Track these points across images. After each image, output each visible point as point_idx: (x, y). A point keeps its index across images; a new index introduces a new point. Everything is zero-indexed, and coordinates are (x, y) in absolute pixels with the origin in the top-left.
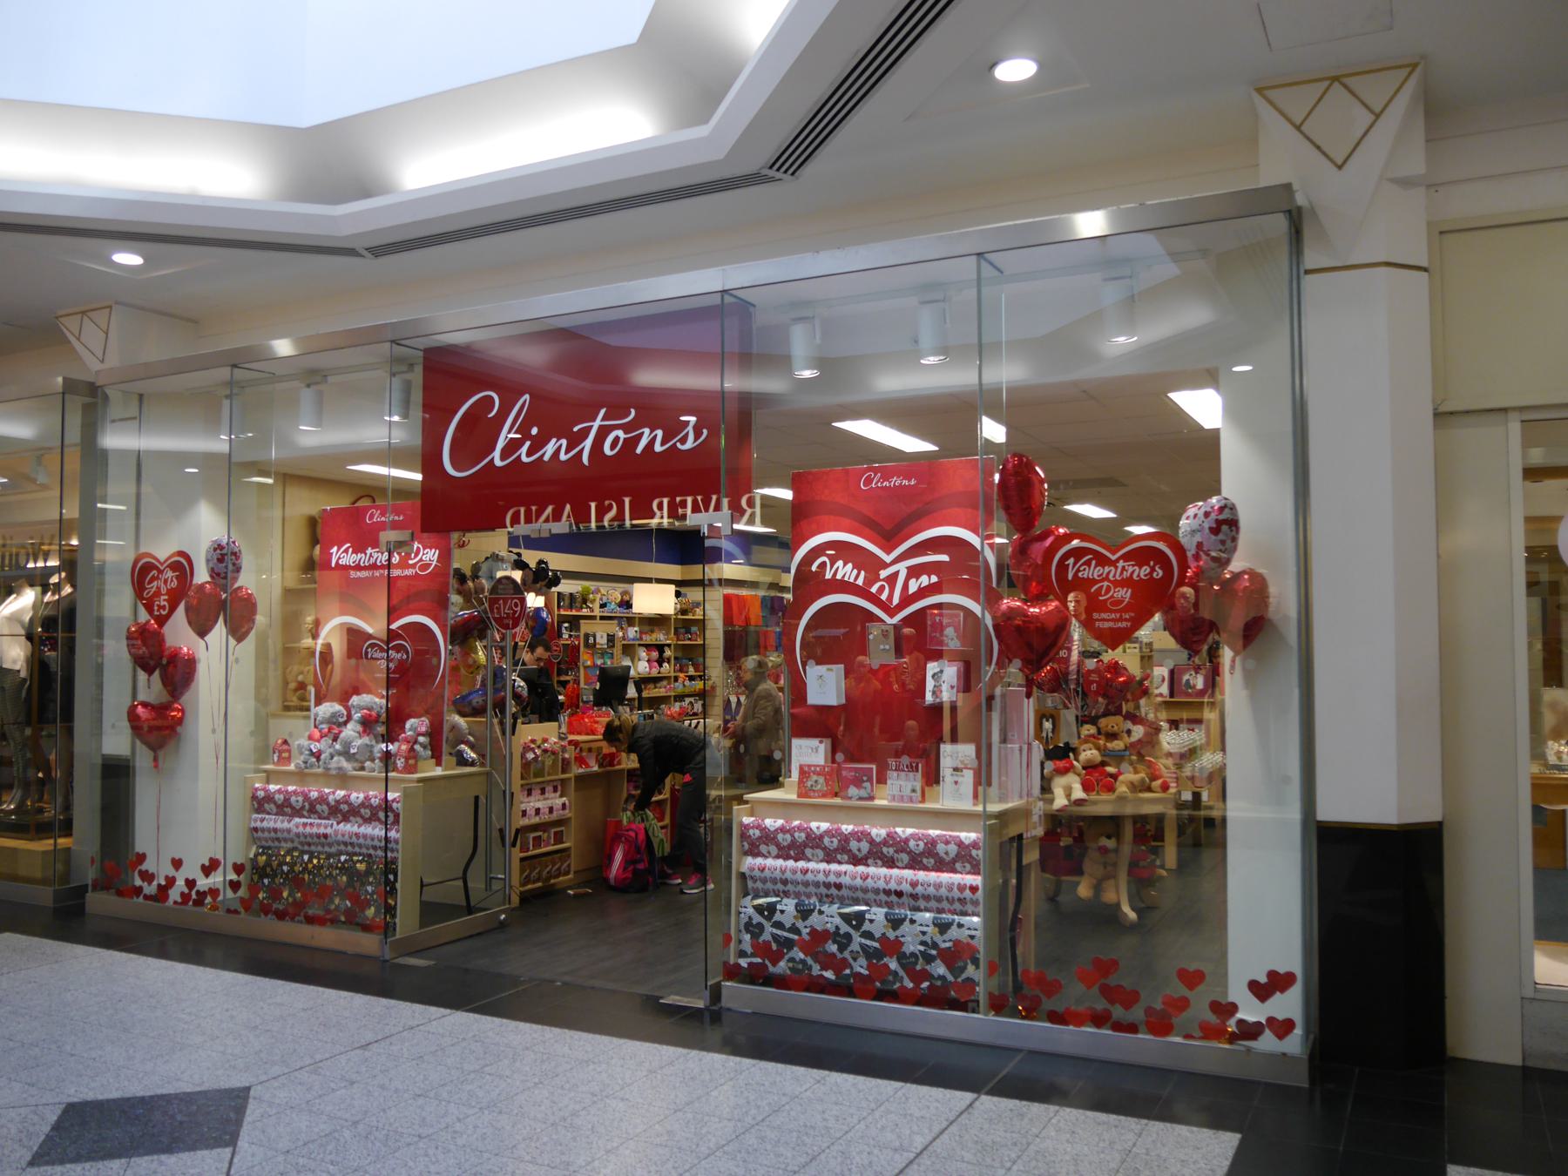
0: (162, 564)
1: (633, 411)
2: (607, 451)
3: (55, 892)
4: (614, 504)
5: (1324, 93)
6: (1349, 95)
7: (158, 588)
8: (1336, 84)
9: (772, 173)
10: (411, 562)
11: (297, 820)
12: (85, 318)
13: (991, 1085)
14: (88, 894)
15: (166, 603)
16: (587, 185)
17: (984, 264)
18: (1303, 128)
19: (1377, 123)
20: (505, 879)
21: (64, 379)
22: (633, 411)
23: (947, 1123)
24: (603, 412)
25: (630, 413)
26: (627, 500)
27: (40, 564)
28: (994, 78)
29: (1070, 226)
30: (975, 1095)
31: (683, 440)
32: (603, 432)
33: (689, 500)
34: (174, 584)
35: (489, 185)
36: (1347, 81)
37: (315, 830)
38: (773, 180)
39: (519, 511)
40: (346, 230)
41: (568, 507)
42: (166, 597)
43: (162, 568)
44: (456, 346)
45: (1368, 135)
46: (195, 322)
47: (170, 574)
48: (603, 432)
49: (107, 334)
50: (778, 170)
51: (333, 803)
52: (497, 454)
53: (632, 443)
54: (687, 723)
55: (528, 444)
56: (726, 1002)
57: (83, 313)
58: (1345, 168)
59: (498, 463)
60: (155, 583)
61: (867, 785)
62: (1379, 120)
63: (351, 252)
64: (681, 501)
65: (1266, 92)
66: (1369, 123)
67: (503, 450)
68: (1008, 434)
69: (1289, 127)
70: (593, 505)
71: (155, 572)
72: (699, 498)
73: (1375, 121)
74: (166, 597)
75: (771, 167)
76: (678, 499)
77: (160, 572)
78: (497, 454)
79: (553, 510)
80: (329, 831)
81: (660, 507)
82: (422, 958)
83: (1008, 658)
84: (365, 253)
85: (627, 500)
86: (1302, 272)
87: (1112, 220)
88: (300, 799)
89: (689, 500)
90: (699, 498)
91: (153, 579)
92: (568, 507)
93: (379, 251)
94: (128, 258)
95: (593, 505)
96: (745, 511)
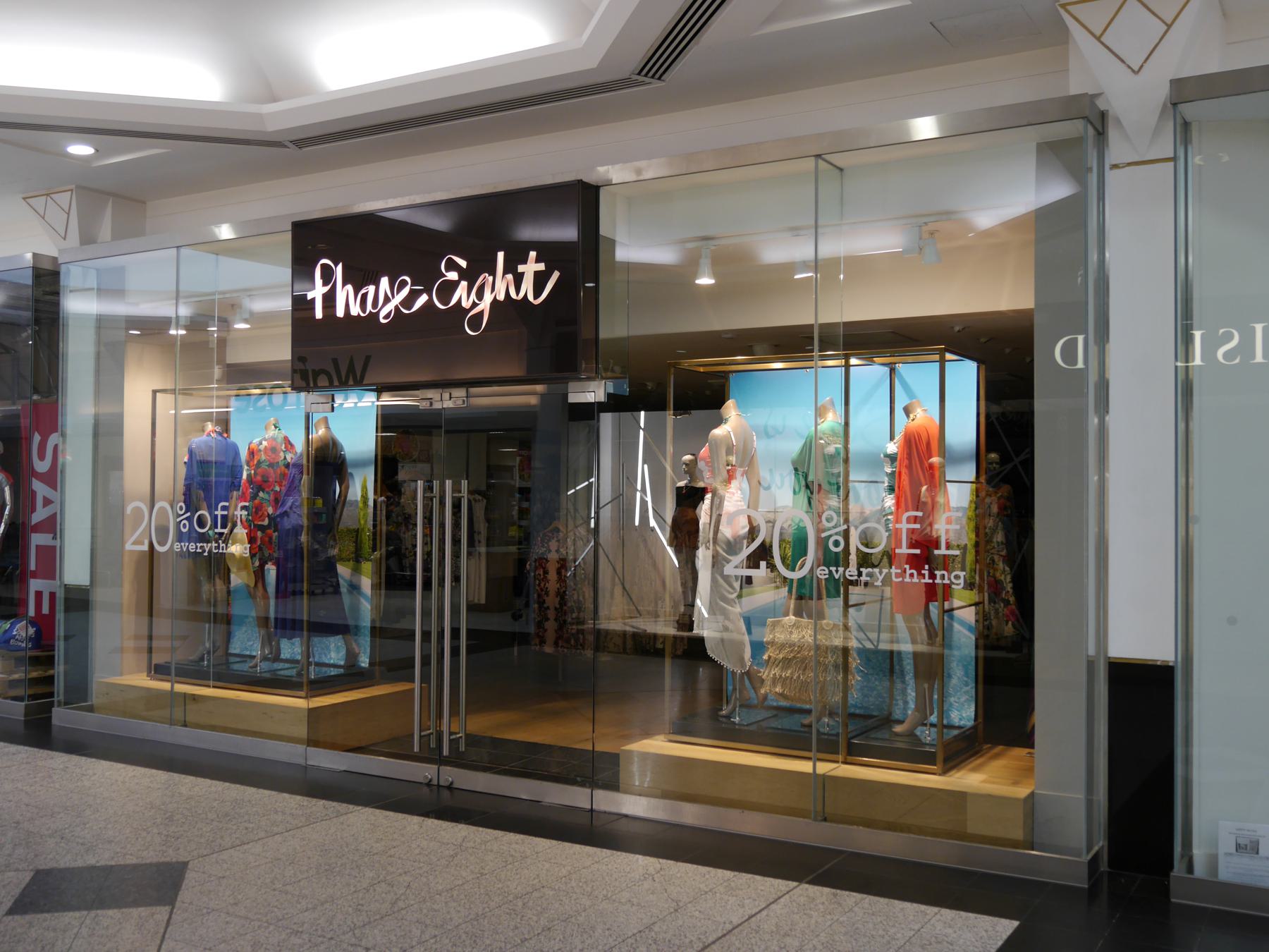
3: (26, 706)
9: (641, 78)
12: (49, 198)
14: (53, 709)
16: (484, 89)
17: (820, 161)
19: (1168, 34)
21: (35, 255)
25: (1223, 333)
26: (1259, 328)
29: (907, 131)
35: (396, 88)
38: (643, 84)
39: (1077, 339)
40: (271, 127)
44: (665, 265)
49: (68, 214)
50: (646, 75)
57: (47, 195)
58: (1140, 73)
65: (1068, 7)
66: (1165, 20)
68: (384, 276)
69: (1170, 31)
73: (1166, 32)
75: (639, 74)
83: (606, 637)
84: (290, 145)
85: (1259, 328)
86: (1107, 167)
87: (941, 125)
93: (301, 143)
94: (80, 149)
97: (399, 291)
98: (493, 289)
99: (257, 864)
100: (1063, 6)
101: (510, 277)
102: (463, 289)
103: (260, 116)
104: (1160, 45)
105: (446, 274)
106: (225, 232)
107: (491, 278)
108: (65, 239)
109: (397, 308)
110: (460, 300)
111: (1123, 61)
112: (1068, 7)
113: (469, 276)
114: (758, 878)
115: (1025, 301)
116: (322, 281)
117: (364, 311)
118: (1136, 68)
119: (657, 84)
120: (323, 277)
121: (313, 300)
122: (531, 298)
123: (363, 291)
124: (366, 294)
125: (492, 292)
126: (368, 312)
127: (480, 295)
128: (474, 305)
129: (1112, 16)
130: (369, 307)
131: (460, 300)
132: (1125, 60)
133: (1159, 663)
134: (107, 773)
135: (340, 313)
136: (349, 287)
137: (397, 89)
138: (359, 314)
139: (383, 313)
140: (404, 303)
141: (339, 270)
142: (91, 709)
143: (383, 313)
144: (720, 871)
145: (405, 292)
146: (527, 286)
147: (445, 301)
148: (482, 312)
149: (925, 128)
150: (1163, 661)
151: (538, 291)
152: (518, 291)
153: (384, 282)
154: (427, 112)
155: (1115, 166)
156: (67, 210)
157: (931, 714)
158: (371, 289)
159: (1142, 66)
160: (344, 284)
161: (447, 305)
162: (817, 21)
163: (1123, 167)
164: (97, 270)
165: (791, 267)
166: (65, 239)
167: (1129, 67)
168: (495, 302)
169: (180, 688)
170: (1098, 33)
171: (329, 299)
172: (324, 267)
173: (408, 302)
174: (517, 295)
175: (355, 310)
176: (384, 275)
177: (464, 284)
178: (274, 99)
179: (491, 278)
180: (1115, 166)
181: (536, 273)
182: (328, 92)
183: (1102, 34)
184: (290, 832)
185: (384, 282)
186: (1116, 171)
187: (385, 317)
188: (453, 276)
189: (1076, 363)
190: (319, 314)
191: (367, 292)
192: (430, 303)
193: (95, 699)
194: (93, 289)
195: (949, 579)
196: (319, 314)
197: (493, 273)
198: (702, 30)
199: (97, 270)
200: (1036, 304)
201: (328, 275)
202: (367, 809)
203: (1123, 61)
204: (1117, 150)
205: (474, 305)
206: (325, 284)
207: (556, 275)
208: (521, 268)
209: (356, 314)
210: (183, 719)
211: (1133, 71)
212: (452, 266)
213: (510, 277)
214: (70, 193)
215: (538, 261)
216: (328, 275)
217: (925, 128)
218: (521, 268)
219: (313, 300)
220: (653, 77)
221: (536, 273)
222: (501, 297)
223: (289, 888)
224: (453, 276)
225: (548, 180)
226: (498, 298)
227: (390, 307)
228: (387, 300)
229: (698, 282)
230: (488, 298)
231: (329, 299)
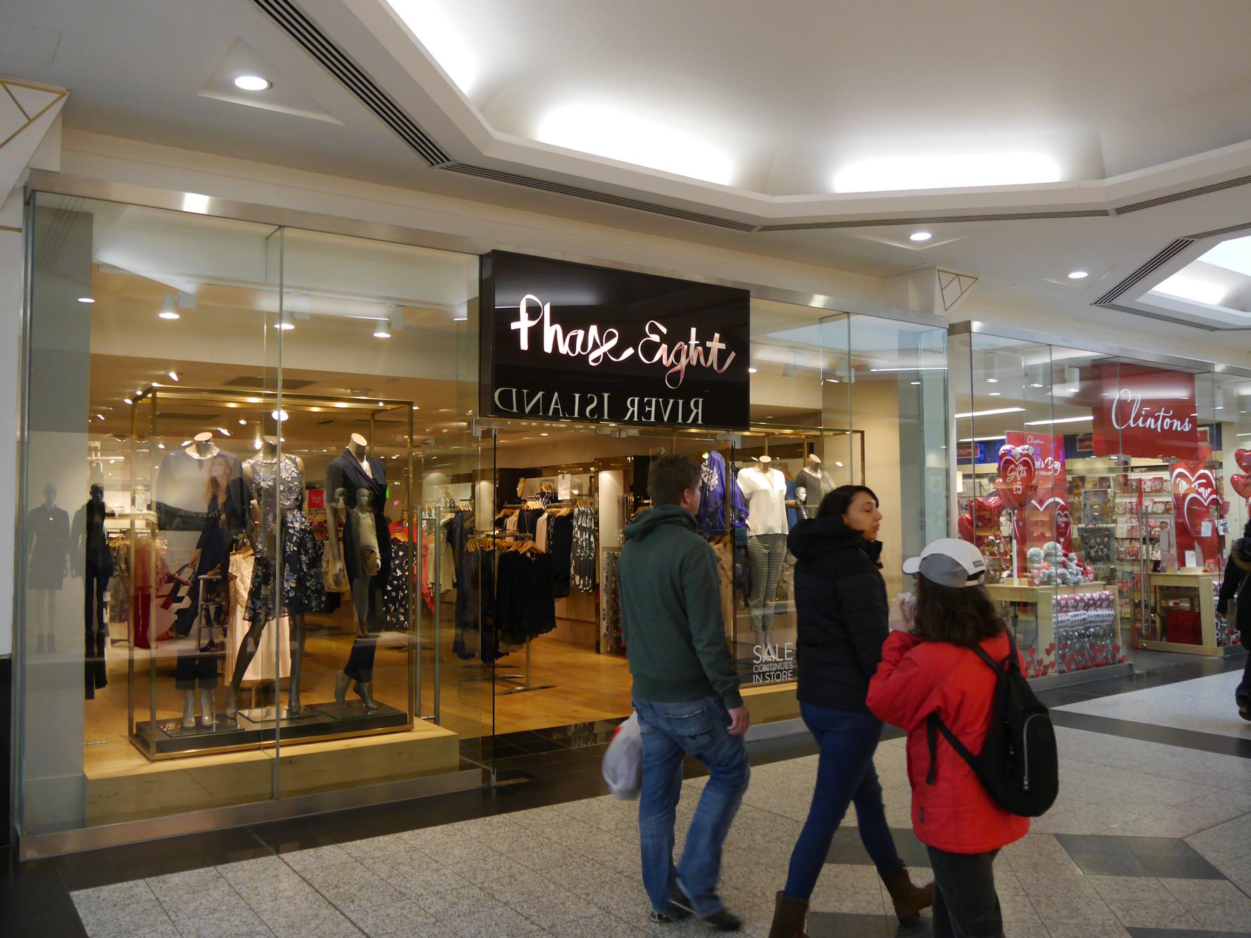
0: (1017, 461)
1: (1171, 411)
2: (1166, 428)
4: (595, 397)
7: (1016, 477)
10: (1049, 468)
11: (1069, 614)
15: (1020, 487)
19: (28, 128)
22: (1171, 411)
24: (1163, 409)
26: (606, 395)
31: (1185, 427)
32: (1164, 418)
33: (654, 400)
34: (1025, 474)
37: (1080, 618)
41: (556, 395)
42: (1020, 483)
43: (1017, 464)
47: (1022, 468)
48: (1164, 418)
51: (1087, 601)
52: (1131, 421)
53: (1172, 424)
54: (497, 532)
55: (1142, 418)
57: (958, 275)
59: (1132, 425)
60: (1013, 473)
64: (648, 400)
67: (1134, 419)
69: (30, 126)
70: (577, 396)
71: (1013, 466)
72: (661, 400)
74: (1020, 483)
76: (646, 399)
77: (1016, 466)
78: (1131, 421)
80: (1085, 616)
81: (633, 405)
85: (606, 395)
87: (212, 206)
88: (1073, 601)
89: (654, 400)
90: (661, 400)
91: (1012, 470)
92: (556, 395)
95: (577, 396)
96: (693, 411)
98: (687, 356)
102: (664, 351)
105: (650, 335)
107: (686, 347)
108: (946, 310)
109: (605, 354)
113: (669, 340)
115: (821, 408)
116: (527, 314)
121: (518, 331)
122: (715, 367)
123: (572, 333)
125: (687, 357)
126: (577, 353)
127: (678, 357)
128: (673, 365)
130: (578, 349)
137: (563, 157)
138: (568, 353)
139: (592, 356)
140: (612, 351)
143: (592, 356)
145: (613, 342)
146: (713, 357)
147: (650, 357)
149: (196, 203)
153: (593, 330)
154: (675, 206)
156: (963, 291)
157: (141, 739)
160: (552, 324)
168: (689, 365)
169: (285, 752)
171: (536, 334)
173: (617, 351)
174: (706, 364)
175: (564, 349)
177: (664, 346)
179: (686, 347)
181: (719, 350)
182: (535, 141)
185: (593, 330)
187: (594, 361)
188: (655, 338)
189: (650, 419)
190: (524, 345)
191: (577, 335)
192: (635, 356)
196: (524, 345)
198: (384, 121)
206: (531, 318)
207: (733, 355)
208: (708, 344)
209: (565, 353)
210: (270, 791)
212: (654, 330)
217: (196, 203)
218: (708, 344)
221: (719, 350)
222: (694, 363)
228: (596, 346)
229: (376, 335)
230: (684, 361)
231: (536, 334)
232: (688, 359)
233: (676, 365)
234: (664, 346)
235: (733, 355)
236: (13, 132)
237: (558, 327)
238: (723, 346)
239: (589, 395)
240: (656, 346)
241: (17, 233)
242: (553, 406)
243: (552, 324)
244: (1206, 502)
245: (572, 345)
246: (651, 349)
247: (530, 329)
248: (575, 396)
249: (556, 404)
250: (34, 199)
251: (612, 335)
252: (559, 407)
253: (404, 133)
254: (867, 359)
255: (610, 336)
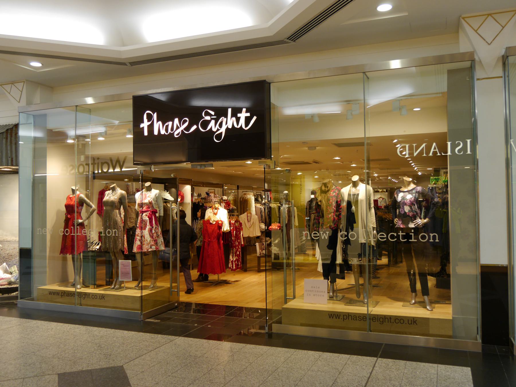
5: (486, 19)
6: (494, 21)
8: (490, 17)
9: (288, 40)
13: (380, 354)
18: (478, 31)
20: (177, 291)
23: (375, 366)
27: (117, 170)
28: (377, 10)
30: (376, 358)
36: (493, 15)
38: (288, 43)
45: (478, 35)
46: (368, 78)
49: (22, 92)
56: (274, 331)
58: (491, 44)
61: (310, 252)
62: (504, 29)
63: (124, 64)
65: (465, 19)
69: (503, 30)
70: (449, 144)
75: (288, 39)
79: (426, 145)
82: (152, 319)
85: (469, 141)
87: (402, 63)
93: (133, 64)
94: (36, 64)
97: (183, 124)
99: (152, 365)
100: (463, 18)
101: (234, 119)
103: (120, 52)
104: (499, 34)
106: (90, 101)
107: (225, 119)
108: (19, 102)
109: (182, 131)
110: (211, 128)
111: (485, 40)
112: (465, 19)
114: (360, 357)
117: (167, 132)
118: (489, 43)
119: (293, 43)
120: (147, 118)
121: (143, 128)
122: (244, 127)
123: (167, 124)
124: (168, 125)
126: (169, 133)
127: (221, 125)
128: (218, 130)
129: (482, 23)
130: (169, 131)
131: (211, 128)
132: (486, 39)
133: (500, 266)
134: (58, 328)
135: (156, 133)
136: (160, 123)
141: (155, 116)
142: (33, 300)
144: (241, 344)
145: (186, 124)
146: (242, 122)
148: (221, 133)
149: (395, 64)
150: (502, 265)
151: (247, 124)
152: (238, 124)
153: (176, 121)
155: (478, 79)
158: (170, 123)
159: (492, 42)
160: (158, 121)
161: (188, 132)
162: (367, 20)
163: (481, 80)
164: (33, 115)
165: (94, 136)
166: (19, 102)
167: (487, 42)
168: (227, 129)
170: (476, 29)
171: (151, 127)
172: (147, 114)
173: (188, 128)
175: (163, 132)
176: (176, 118)
177: (213, 122)
178: (124, 45)
179: (225, 119)
180: (478, 79)
183: (478, 29)
184: (157, 349)
185: (176, 121)
186: (478, 81)
187: (177, 135)
188: (208, 118)
190: (146, 134)
192: (197, 129)
193: (35, 294)
194: (32, 123)
195: (429, 236)
196: (146, 134)
197: (226, 116)
199: (33, 115)
200: (449, 130)
201: (150, 117)
202: (181, 338)
203: (485, 40)
204: (479, 73)
205: (218, 130)
206: (148, 121)
207: (255, 118)
208: (239, 115)
209: (163, 134)
211: (488, 44)
213: (234, 119)
214: (23, 83)
215: (247, 112)
216: (150, 117)
217: (395, 64)
218: (239, 115)
219: (143, 128)
220: (292, 40)
223: (174, 374)
224: (208, 118)
225: (227, 83)
226: (229, 127)
227: (179, 130)
228: (178, 128)
230: (224, 127)
231: (151, 127)
232: (227, 125)
233: (220, 130)
234: (213, 122)
235: (255, 118)
236: (497, 34)
237: (160, 123)
238: (248, 115)
239: (457, 142)
240: (209, 122)
241: (500, 79)
242: (432, 150)
243: (158, 121)
244: (477, 340)
245: (167, 130)
246: (206, 124)
247: (148, 126)
248: (467, 141)
249: (435, 148)
250: (508, 61)
251: (185, 121)
252: (437, 150)
253: (316, 24)
254: (64, 129)
255: (185, 121)
